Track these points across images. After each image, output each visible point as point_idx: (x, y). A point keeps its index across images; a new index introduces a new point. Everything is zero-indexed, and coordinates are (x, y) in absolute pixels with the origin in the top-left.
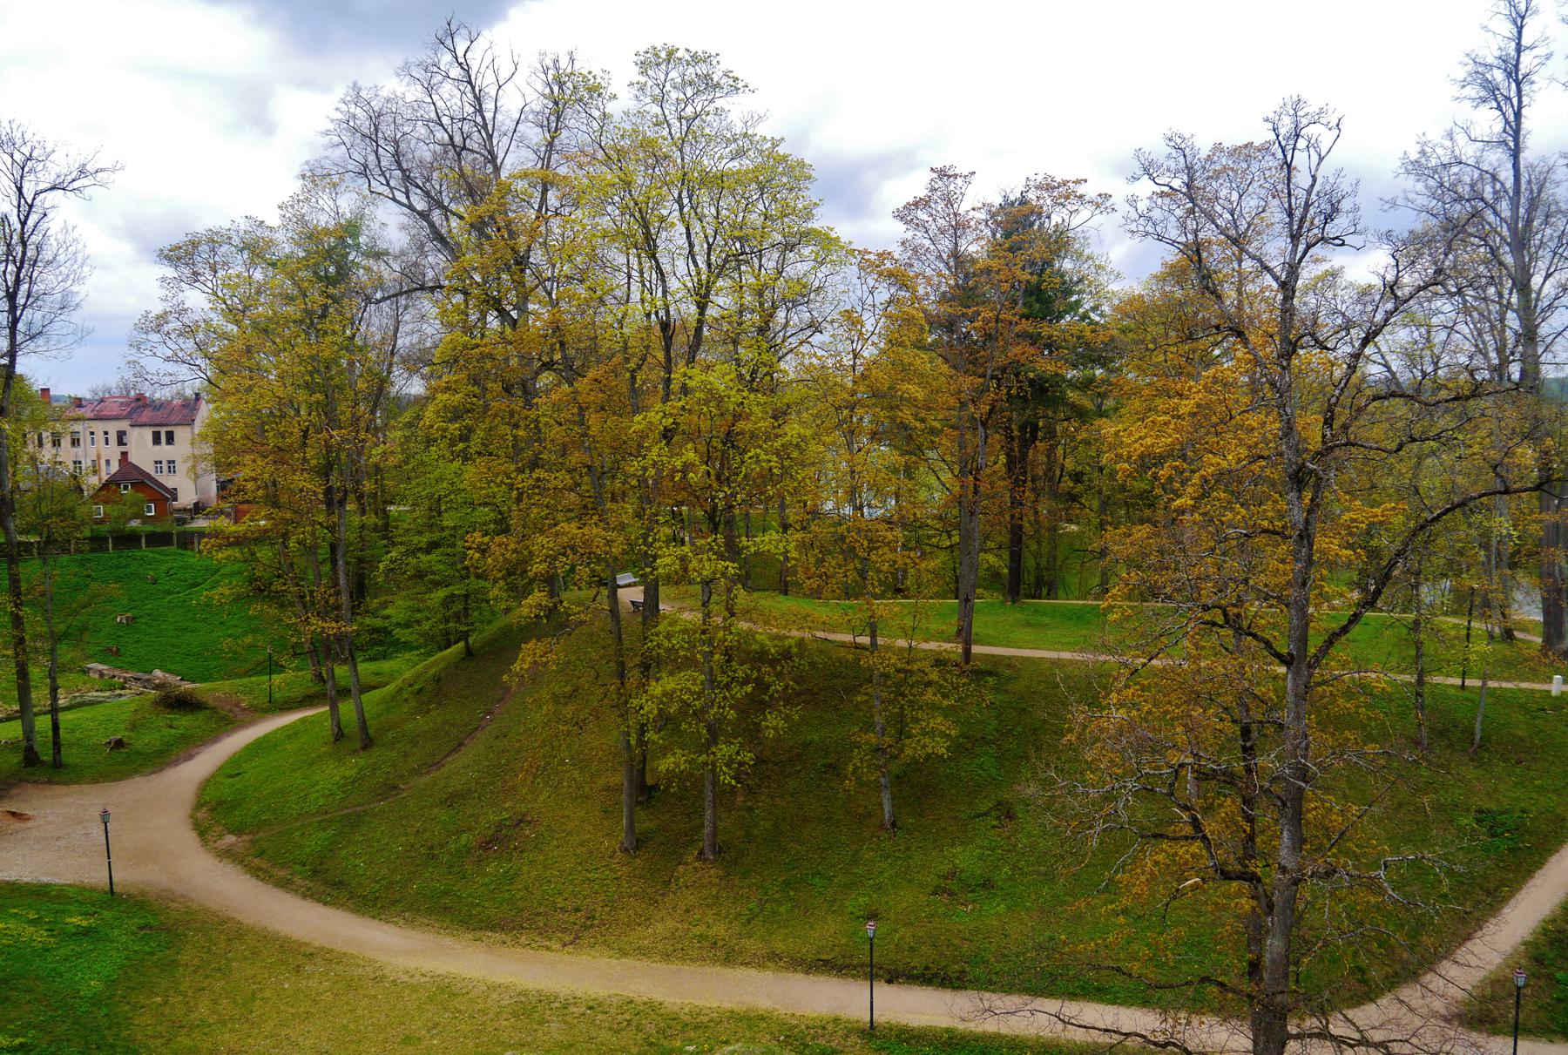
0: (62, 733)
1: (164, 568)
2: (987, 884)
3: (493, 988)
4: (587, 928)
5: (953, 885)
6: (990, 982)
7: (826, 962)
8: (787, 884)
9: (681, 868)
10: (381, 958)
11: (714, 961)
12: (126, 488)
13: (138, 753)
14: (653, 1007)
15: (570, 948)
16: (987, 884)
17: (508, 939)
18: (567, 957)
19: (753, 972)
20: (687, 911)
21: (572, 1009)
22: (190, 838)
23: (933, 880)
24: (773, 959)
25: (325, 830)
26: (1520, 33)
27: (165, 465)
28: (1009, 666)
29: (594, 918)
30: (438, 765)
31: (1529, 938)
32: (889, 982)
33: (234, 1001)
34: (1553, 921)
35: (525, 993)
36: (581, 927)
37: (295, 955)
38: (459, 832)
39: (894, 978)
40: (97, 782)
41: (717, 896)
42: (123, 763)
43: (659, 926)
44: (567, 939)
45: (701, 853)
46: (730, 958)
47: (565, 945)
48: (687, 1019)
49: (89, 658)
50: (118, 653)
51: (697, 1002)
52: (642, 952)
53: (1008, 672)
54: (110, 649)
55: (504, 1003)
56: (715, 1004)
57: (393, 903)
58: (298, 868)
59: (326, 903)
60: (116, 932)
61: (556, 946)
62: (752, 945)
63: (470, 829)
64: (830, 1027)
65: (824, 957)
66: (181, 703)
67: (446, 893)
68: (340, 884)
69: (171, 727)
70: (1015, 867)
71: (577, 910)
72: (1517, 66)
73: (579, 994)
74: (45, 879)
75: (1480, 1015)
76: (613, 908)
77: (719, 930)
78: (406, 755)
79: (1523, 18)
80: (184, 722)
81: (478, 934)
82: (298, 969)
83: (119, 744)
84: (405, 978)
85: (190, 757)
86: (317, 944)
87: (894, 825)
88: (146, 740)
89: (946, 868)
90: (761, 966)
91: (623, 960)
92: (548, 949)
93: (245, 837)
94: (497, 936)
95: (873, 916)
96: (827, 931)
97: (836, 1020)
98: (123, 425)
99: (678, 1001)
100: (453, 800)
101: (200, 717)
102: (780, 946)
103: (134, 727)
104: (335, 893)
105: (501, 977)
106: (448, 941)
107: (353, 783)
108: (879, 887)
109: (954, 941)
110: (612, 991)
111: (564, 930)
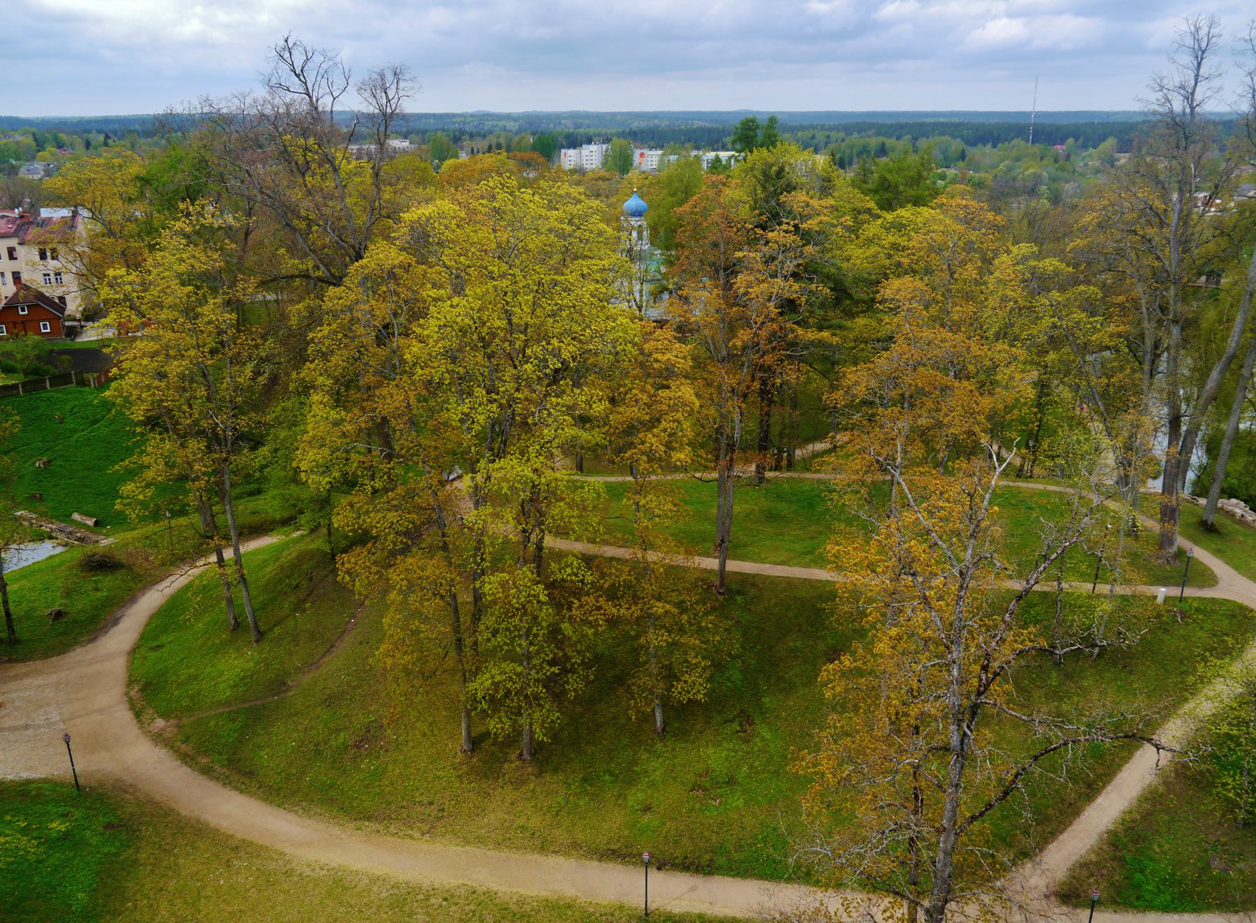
0: (11, 605)
1: (70, 405)
2: (731, 781)
3: (376, 880)
4: (439, 819)
5: (705, 782)
6: (731, 869)
7: (614, 851)
8: (584, 780)
9: (506, 765)
10: (288, 850)
11: (533, 849)
12: (23, 310)
13: (76, 622)
14: (490, 895)
15: (427, 837)
16: (731, 781)
17: (380, 827)
18: (425, 846)
19: (560, 860)
20: (512, 804)
21: (433, 901)
22: (126, 716)
23: (691, 777)
24: (574, 848)
25: (233, 720)
26: (1199, 64)
27: (52, 277)
28: (753, 585)
29: (443, 810)
30: (315, 665)
31: (1112, 827)
32: (659, 869)
33: (186, 902)
34: (1130, 812)
35: (396, 886)
36: (437, 820)
37: (229, 848)
38: (338, 730)
39: (663, 864)
40: (47, 657)
41: (533, 791)
42: (64, 633)
43: (492, 816)
44: (426, 828)
45: (521, 755)
46: (545, 847)
47: (423, 834)
48: (514, 908)
49: (17, 506)
50: (41, 499)
51: (522, 891)
52: (481, 841)
53: (752, 592)
54: (34, 496)
55: (383, 895)
56: (535, 893)
57: (293, 793)
58: (216, 757)
59: (241, 792)
60: (88, 833)
61: (417, 835)
62: (561, 835)
63: (346, 728)
64: (616, 913)
65: (613, 847)
66: (101, 565)
67: (331, 786)
68: (250, 774)
69: (97, 590)
70: (751, 767)
71: (431, 804)
72: (1193, 94)
73: (437, 885)
74: (25, 775)
75: (1070, 894)
76: (458, 802)
77: (535, 822)
78: (290, 653)
79: (1203, 52)
80: (108, 582)
81: (359, 823)
82: (228, 864)
83: (59, 615)
84: (308, 871)
85: (116, 622)
86: (239, 836)
87: (663, 730)
88: (80, 604)
89: (701, 767)
90: (567, 855)
91: (467, 848)
92: (411, 837)
93: (172, 721)
94: (373, 826)
95: (647, 809)
96: (612, 823)
97: (621, 907)
98: (13, 242)
99: (509, 890)
100: (330, 701)
101: (120, 574)
102: (580, 837)
103: (68, 594)
104: (247, 781)
105: (379, 870)
106: (337, 831)
107: (252, 676)
108: (652, 784)
109: (706, 834)
110: (461, 881)
111: (422, 821)
